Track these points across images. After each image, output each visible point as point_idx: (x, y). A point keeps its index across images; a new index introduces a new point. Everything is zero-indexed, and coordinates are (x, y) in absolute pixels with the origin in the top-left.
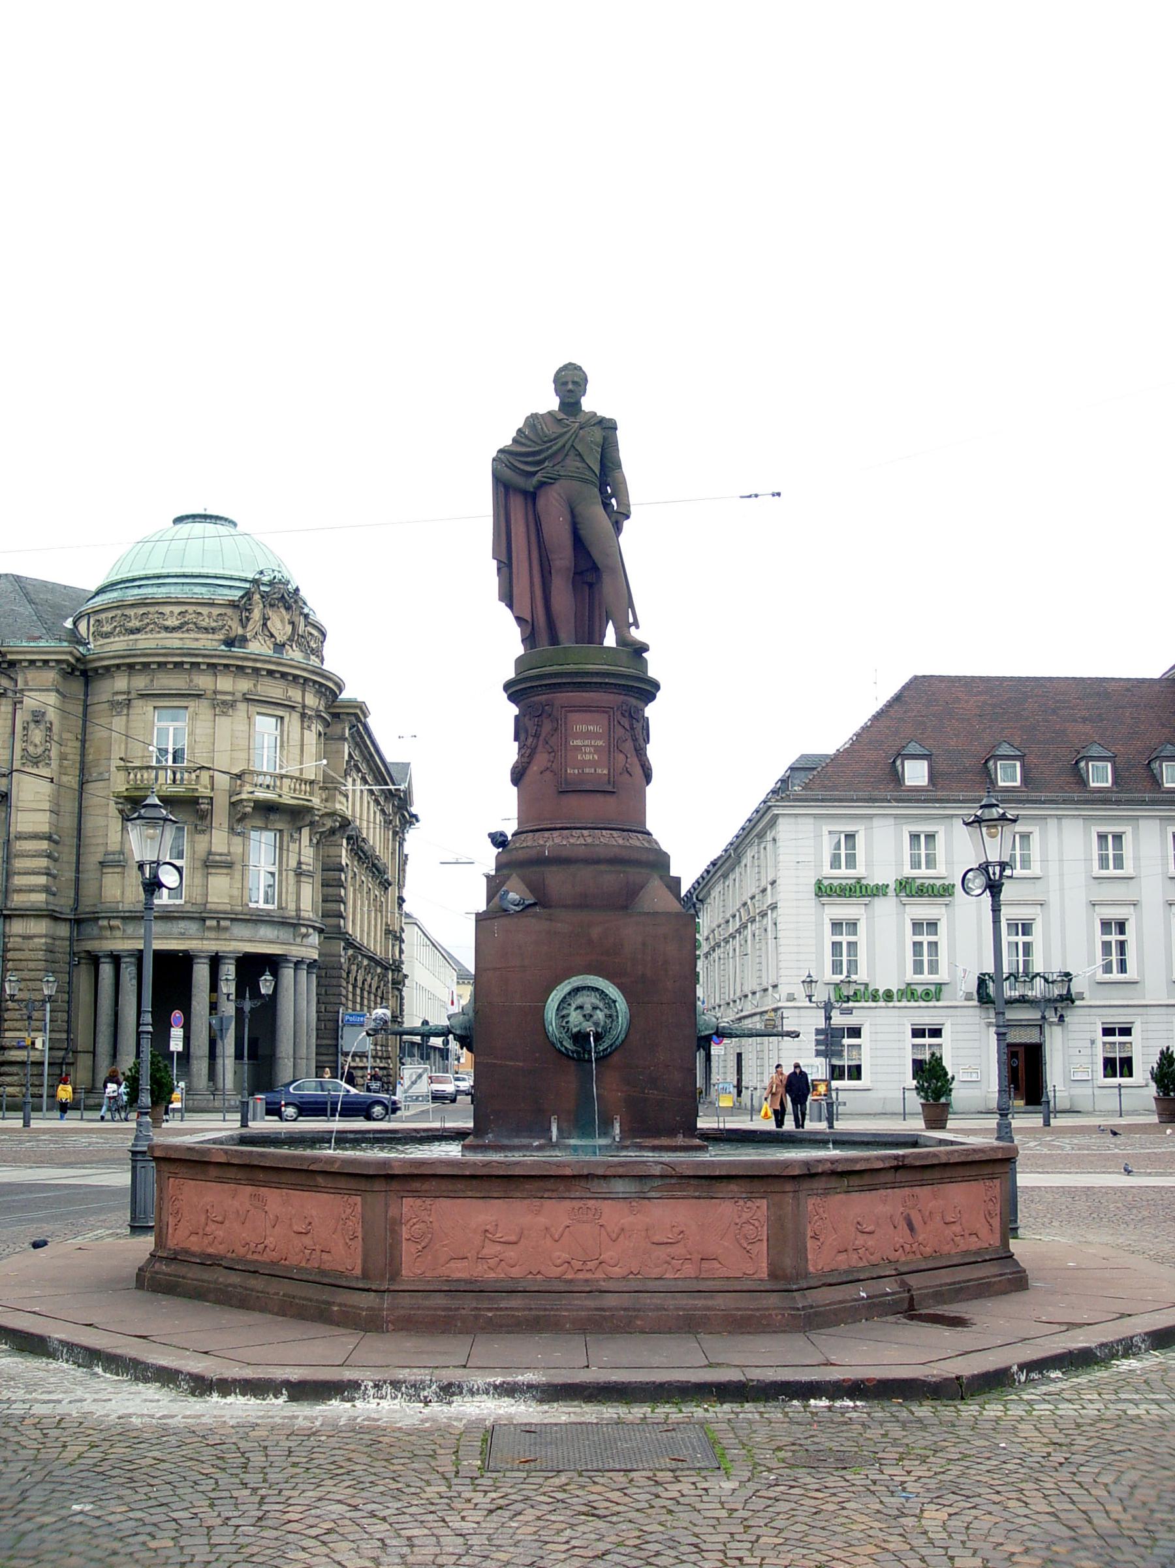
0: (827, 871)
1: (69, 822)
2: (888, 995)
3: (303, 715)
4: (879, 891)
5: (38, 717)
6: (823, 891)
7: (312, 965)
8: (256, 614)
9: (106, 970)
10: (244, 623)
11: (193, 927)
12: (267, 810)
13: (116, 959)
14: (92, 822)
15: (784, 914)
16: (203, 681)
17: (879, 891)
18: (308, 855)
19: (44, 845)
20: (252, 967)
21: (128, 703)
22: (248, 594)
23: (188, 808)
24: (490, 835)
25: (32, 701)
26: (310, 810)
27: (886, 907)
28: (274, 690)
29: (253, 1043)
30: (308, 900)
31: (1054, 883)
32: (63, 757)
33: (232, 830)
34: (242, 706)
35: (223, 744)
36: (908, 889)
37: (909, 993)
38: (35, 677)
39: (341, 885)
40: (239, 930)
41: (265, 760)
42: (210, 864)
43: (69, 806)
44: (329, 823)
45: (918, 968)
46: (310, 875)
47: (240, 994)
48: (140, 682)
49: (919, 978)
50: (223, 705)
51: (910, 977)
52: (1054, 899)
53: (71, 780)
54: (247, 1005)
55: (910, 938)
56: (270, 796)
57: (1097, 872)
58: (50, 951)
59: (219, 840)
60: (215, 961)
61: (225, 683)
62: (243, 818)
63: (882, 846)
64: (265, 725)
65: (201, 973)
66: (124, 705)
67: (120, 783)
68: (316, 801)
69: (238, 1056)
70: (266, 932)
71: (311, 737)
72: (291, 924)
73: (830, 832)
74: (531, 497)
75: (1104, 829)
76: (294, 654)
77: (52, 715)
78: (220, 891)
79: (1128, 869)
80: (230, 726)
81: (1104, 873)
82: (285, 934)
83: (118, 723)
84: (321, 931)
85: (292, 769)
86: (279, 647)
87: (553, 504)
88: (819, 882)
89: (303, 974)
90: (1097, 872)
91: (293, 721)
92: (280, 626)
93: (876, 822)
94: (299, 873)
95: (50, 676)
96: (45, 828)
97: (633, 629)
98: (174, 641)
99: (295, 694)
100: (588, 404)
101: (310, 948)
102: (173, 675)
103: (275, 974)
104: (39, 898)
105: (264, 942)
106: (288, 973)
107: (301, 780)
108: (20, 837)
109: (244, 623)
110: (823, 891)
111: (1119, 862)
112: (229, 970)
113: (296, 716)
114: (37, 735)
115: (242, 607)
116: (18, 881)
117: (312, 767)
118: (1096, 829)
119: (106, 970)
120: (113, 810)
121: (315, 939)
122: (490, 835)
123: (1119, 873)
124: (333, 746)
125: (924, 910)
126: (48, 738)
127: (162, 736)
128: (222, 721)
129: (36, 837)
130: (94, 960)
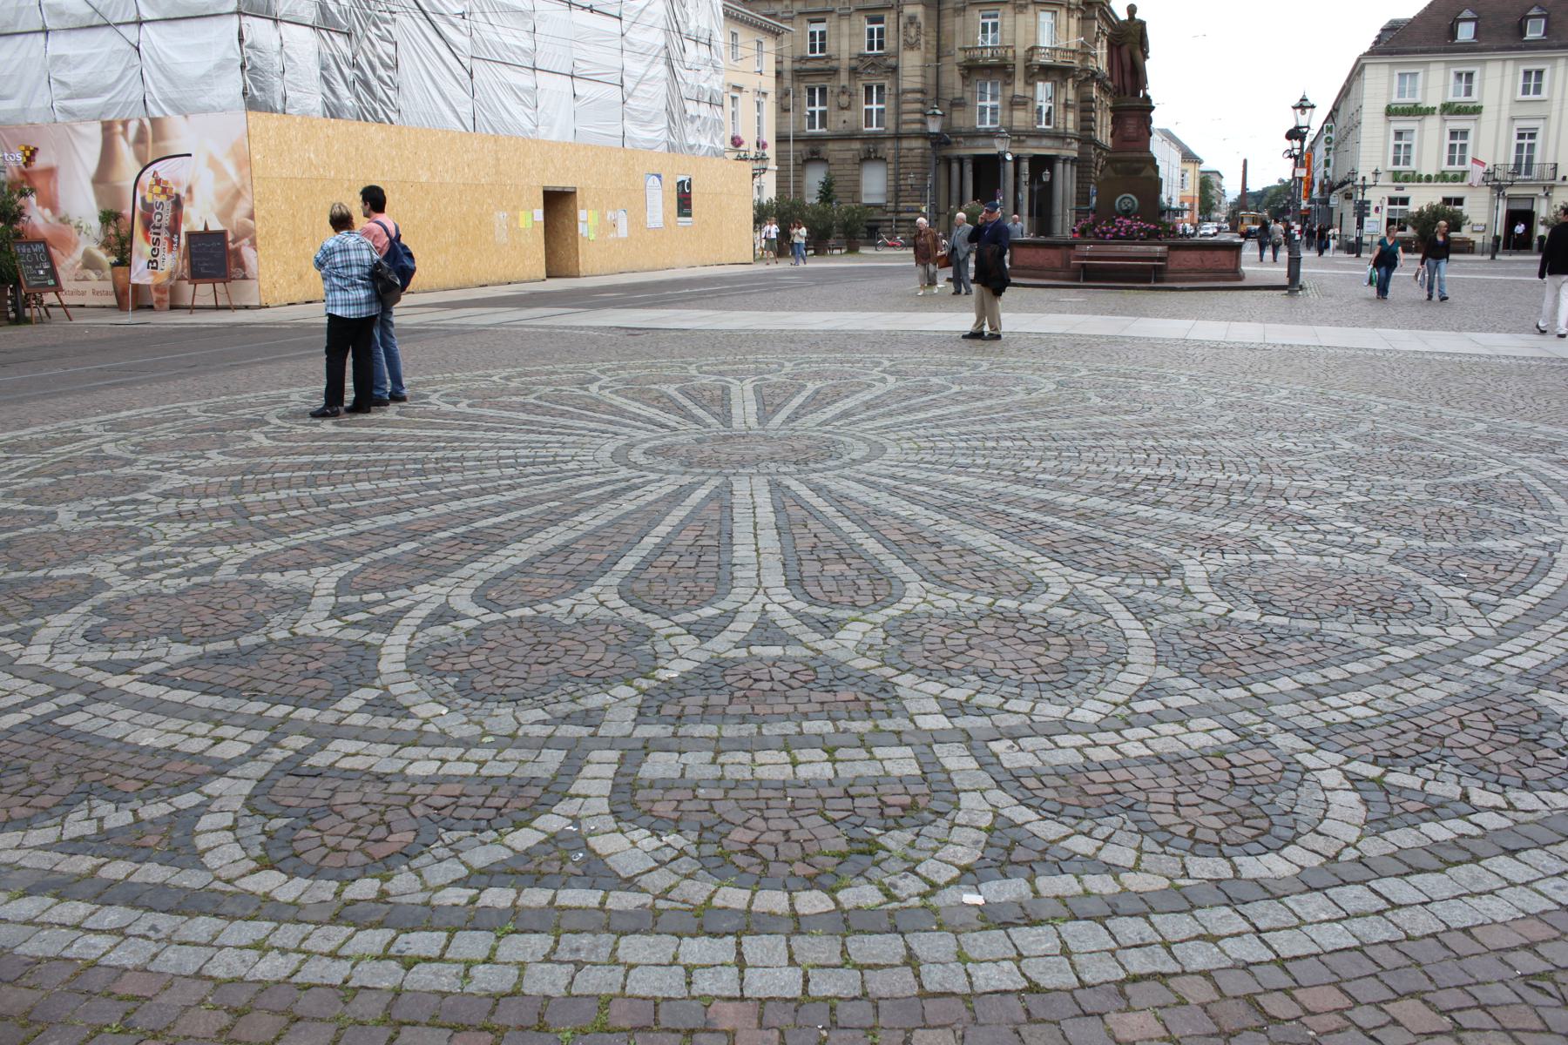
0: (1395, 99)
1: (931, 81)
2: (1429, 179)
3: (1069, 9)
4: (1429, 111)
5: (912, 20)
6: (1477, 110)
7: (1074, 161)
9: (955, 167)
12: (1047, 71)
13: (961, 160)
15: (1365, 130)
17: (1429, 111)
18: (1071, 95)
19: (919, 96)
20: (1041, 164)
21: (964, 9)
23: (1000, 70)
26: (1073, 69)
27: (1433, 122)
29: (1039, 206)
30: (1071, 122)
31: (1556, 107)
32: (927, 43)
33: (1027, 83)
34: (1031, 7)
35: (1020, 33)
36: (1449, 109)
37: (1443, 177)
39: (1092, 110)
40: (1031, 142)
41: (1045, 40)
42: (1015, 103)
43: (931, 73)
44: (1084, 75)
45: (1451, 161)
46: (1073, 107)
47: (1031, 181)
49: (1452, 168)
51: (1445, 167)
52: (1554, 115)
53: (932, 56)
54: (1036, 188)
55: (1447, 141)
56: (1049, 61)
57: (1519, 96)
58: (923, 156)
59: (1019, 88)
62: (1033, 75)
63: (1435, 82)
64: (1046, 18)
67: (960, 57)
69: (1031, 214)
70: (1045, 142)
71: (1073, 22)
72: (1060, 137)
74: (1119, 48)
75: (1529, 67)
77: (921, 19)
78: (1021, 118)
79: (1544, 94)
81: (1526, 97)
82: (1057, 143)
83: (959, 21)
84: (1079, 140)
85: (1062, 44)
87: (1125, 50)
88: (1389, 107)
89: (1068, 166)
90: (1519, 96)
91: (1063, 14)
93: (1432, 66)
94: (1066, 106)
96: (919, 86)
100: (1137, 16)
101: (1072, 151)
103: (1052, 171)
104: (917, 126)
105: (1045, 148)
106: (1059, 166)
107: (1067, 51)
108: (905, 92)
110: (1391, 112)
111: (1538, 90)
113: (1064, 12)
114: (913, 32)
116: (905, 117)
117: (1074, 42)
118: (1522, 68)
119: (955, 167)
121: (1075, 145)
123: (1537, 97)
124: (1088, 23)
125: (1458, 123)
126: (918, 33)
128: (1020, 17)
129: (914, 91)
130: (948, 161)
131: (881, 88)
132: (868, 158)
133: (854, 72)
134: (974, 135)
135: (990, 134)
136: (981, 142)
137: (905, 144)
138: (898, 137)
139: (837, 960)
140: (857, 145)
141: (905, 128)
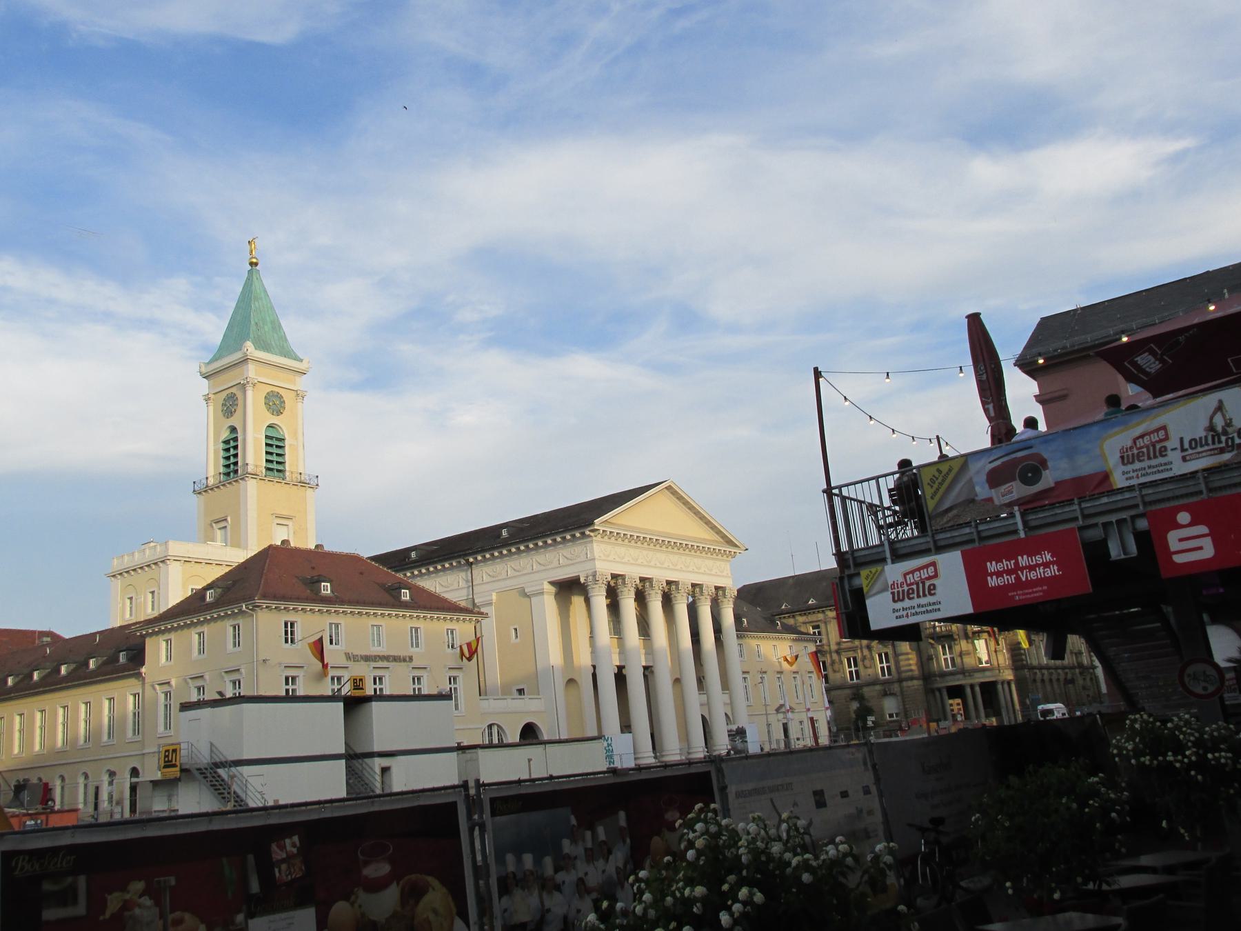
9: (937, 694)
11: (961, 676)
13: (939, 690)
40: (977, 675)
60: (972, 686)
65: (968, 690)
112: (977, 689)
119: (937, 694)
130: (933, 691)
131: (886, 654)
132: (885, 694)
133: (838, 652)
134: (943, 675)
135: (952, 674)
136: (949, 678)
137: (905, 684)
138: (900, 681)
139: (595, 734)
140: (878, 687)
141: (904, 675)
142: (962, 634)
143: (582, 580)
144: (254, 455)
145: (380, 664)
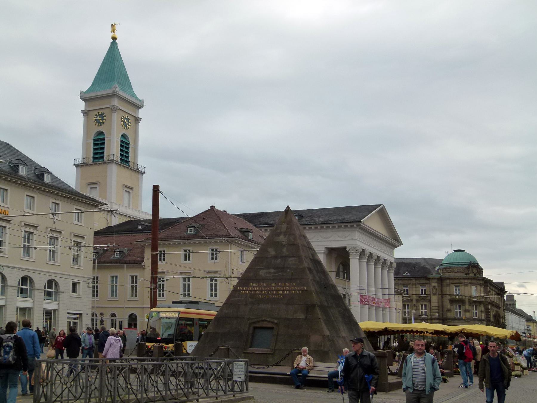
1: (440, 304)
5: (434, 287)
8: (471, 269)
10: (468, 271)
14: (445, 303)
16: (462, 281)
21: (449, 285)
22: (469, 266)
24: (288, 207)
25: (433, 284)
28: (474, 281)
38: (433, 281)
41: (474, 293)
42: (466, 311)
48: (451, 281)
50: (466, 285)
61: (466, 281)
64: (474, 288)
66: (449, 285)
68: (484, 300)
73: (27, 195)
76: (478, 275)
80: (468, 288)
83: (448, 288)
86: (475, 275)
91: (479, 287)
92: (475, 271)
94: (481, 312)
95: (436, 281)
97: (66, 335)
98: (457, 275)
99: (479, 282)
102: (457, 282)
109: (468, 271)
114: (434, 290)
115: (468, 268)
120: (448, 302)
122: (288, 207)
127: (456, 292)
128: (466, 287)
131: (425, 305)
142: (467, 301)
143: (348, 249)
144: (113, 149)
145: (55, 275)
